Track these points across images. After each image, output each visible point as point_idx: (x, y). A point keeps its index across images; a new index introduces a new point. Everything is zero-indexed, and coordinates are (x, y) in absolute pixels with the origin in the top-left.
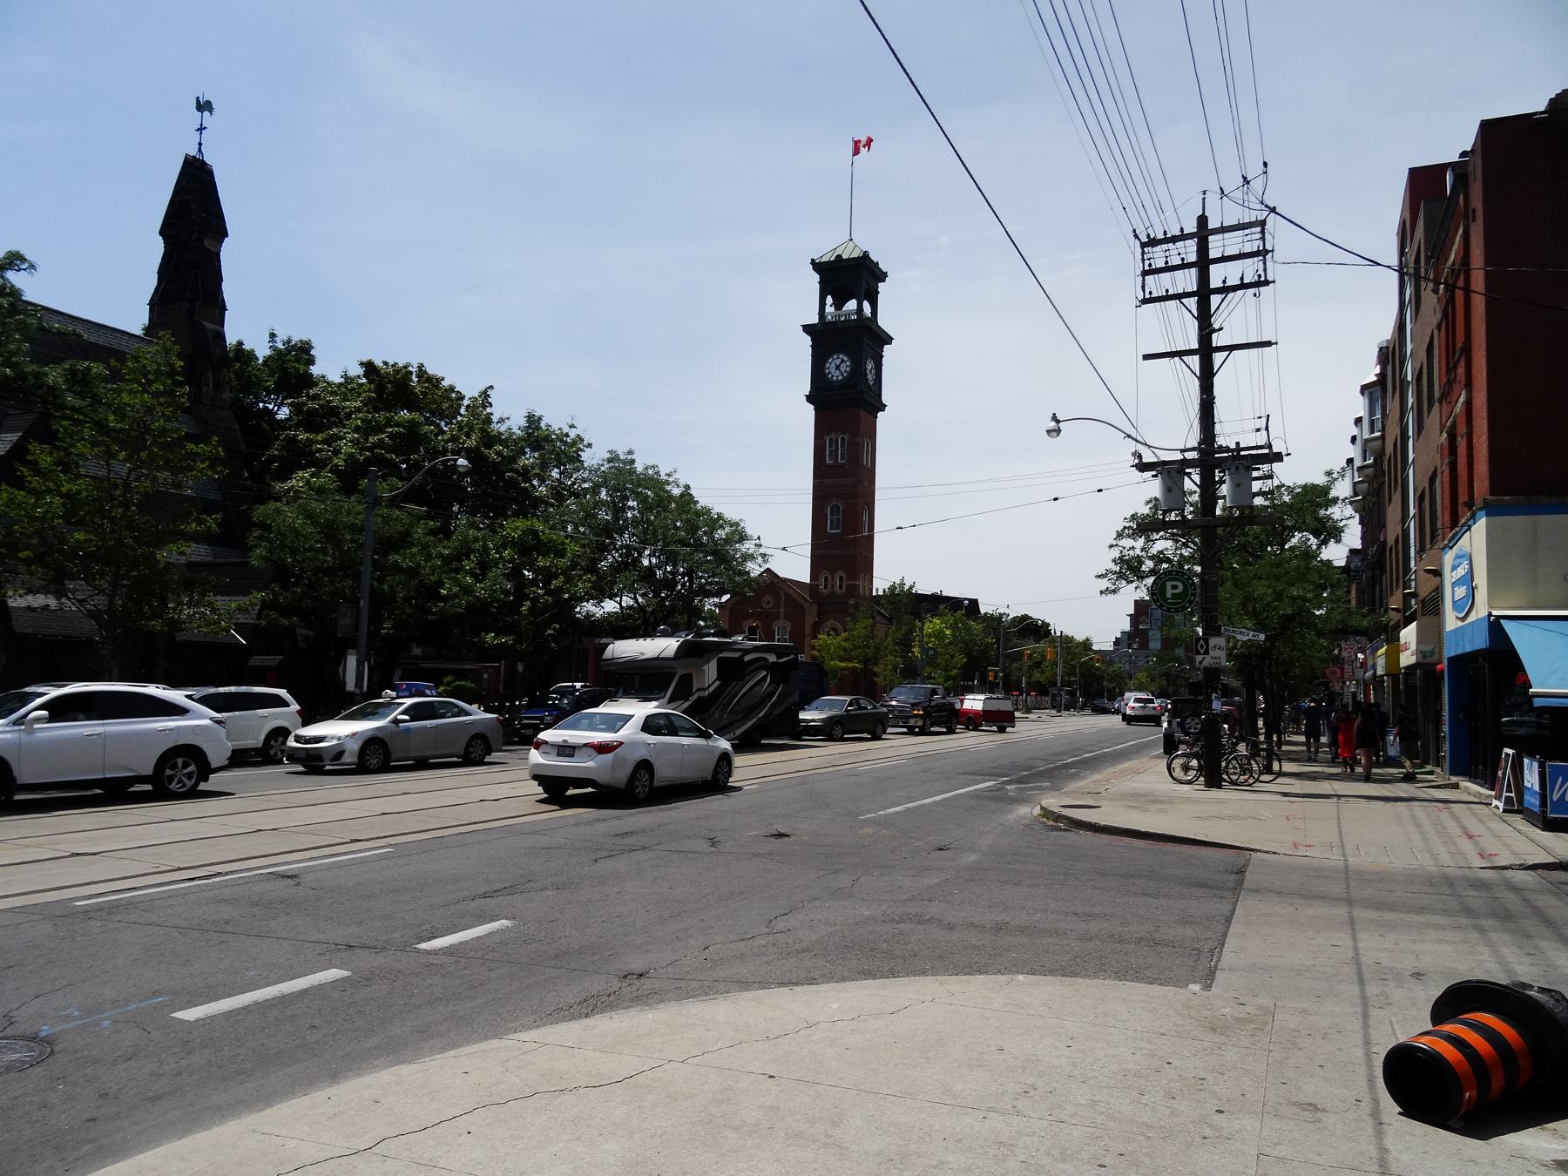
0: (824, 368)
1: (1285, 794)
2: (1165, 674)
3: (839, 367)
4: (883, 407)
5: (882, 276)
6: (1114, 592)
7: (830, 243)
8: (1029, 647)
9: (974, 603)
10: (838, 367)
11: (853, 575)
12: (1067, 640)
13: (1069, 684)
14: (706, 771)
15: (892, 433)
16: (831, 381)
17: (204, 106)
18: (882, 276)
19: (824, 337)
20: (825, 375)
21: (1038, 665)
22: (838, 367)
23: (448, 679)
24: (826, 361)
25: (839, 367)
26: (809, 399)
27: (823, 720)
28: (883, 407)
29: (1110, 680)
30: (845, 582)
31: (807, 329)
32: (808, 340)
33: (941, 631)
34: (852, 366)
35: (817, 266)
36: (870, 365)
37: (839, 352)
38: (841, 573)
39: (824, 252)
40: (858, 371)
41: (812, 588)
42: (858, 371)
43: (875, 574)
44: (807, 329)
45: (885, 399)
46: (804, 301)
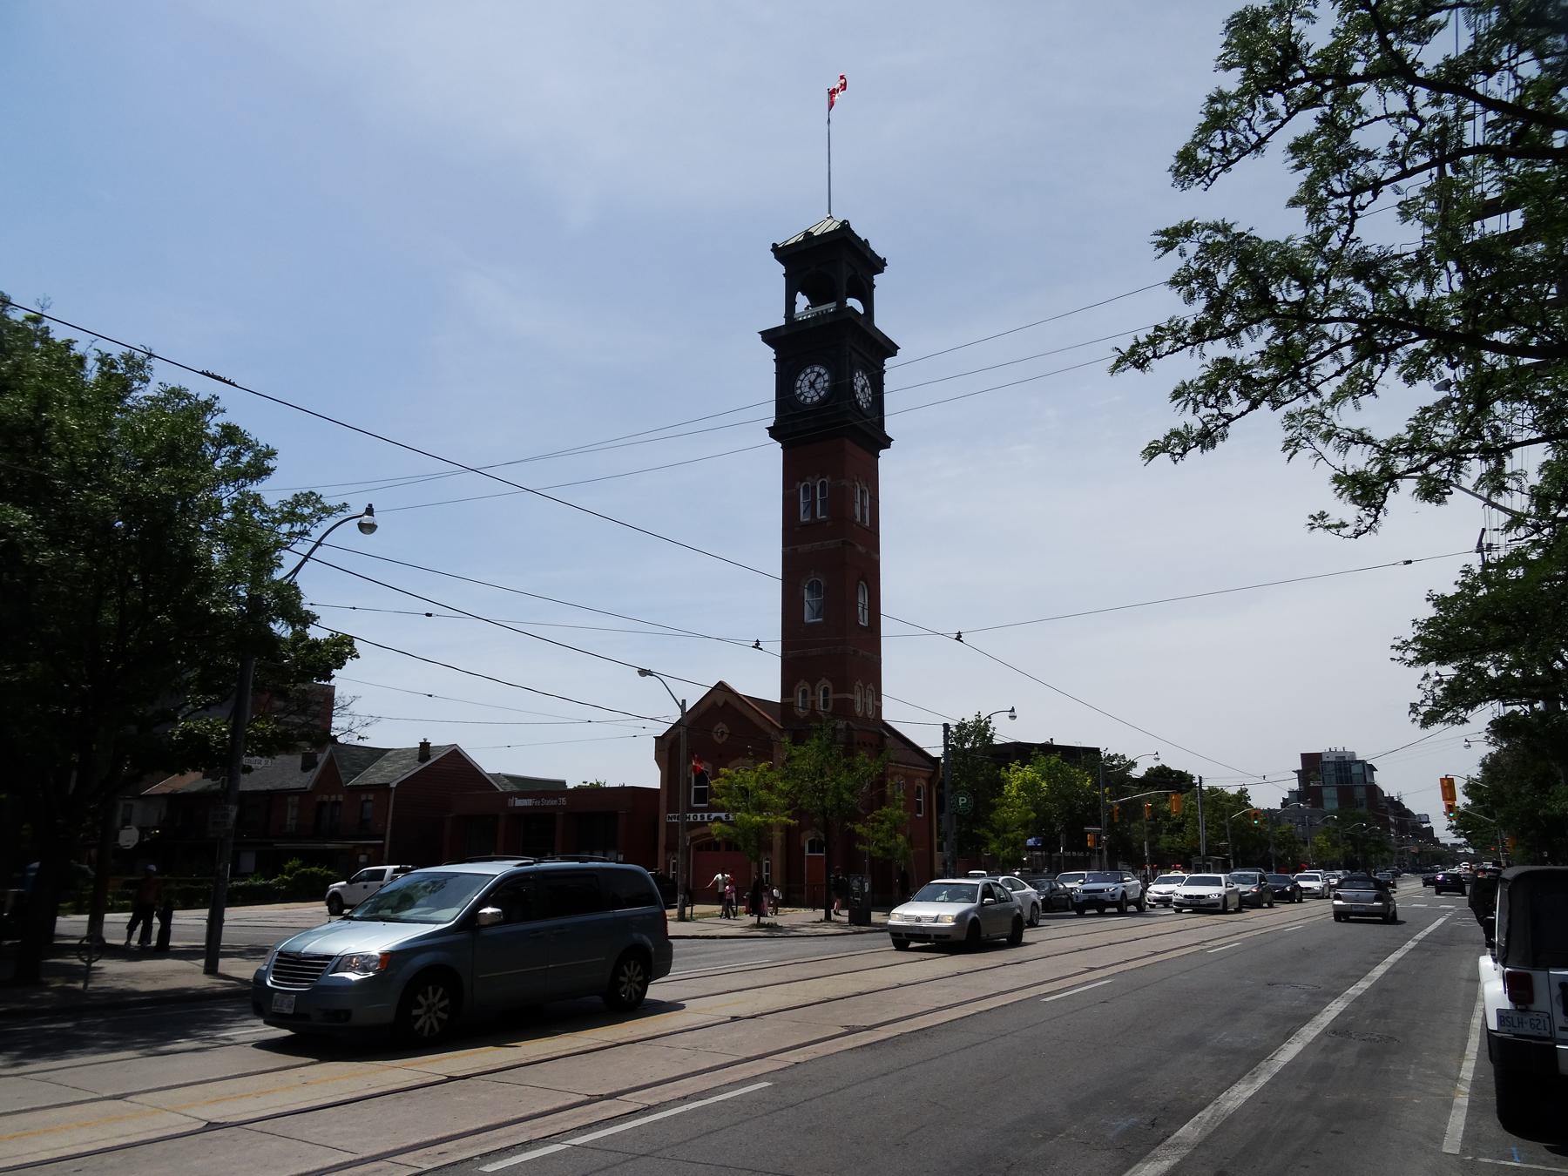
0: (793, 388)
2: (1350, 837)
3: (813, 384)
4: (886, 442)
5: (878, 265)
6: (1207, 439)
8: (1174, 805)
9: (1097, 751)
10: (812, 385)
11: (843, 685)
12: (1216, 796)
13: (1219, 852)
15: (910, 489)
18: (878, 265)
19: (789, 344)
20: (796, 398)
21: (1179, 827)
22: (812, 385)
23: (295, 863)
24: (796, 378)
25: (813, 384)
26: (774, 432)
28: (886, 442)
29: (1279, 846)
30: (831, 696)
31: (769, 336)
32: (770, 353)
33: (1034, 783)
34: (831, 380)
35: (781, 253)
36: (860, 381)
37: (812, 363)
38: (826, 683)
39: (790, 234)
40: (841, 390)
41: (785, 707)
42: (841, 390)
44: (769, 336)
45: (889, 429)
46: (768, 298)
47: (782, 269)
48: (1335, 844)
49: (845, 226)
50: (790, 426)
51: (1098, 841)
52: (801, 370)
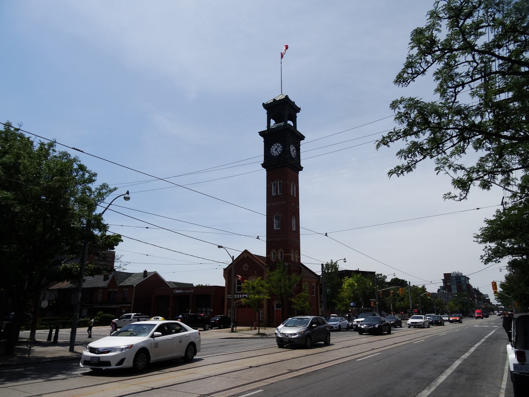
0: (270, 151)
1: (373, 349)
2: (461, 302)
3: (276, 150)
4: (301, 169)
5: (298, 110)
7: (275, 94)
10: (276, 150)
12: (415, 288)
14: (181, 353)
16: (273, 156)
17: (287, 47)
18: (298, 110)
20: (271, 154)
21: (403, 299)
22: (276, 150)
26: (263, 165)
27: (299, 333)
28: (301, 169)
29: (437, 305)
30: (283, 255)
31: (262, 134)
32: (262, 139)
34: (283, 148)
35: (265, 106)
36: (292, 148)
37: (276, 142)
38: (281, 250)
39: (269, 100)
40: (286, 151)
41: (268, 259)
42: (286, 151)
43: (302, 252)
44: (262, 134)
45: (302, 164)
46: (261, 121)
47: (266, 111)
48: (456, 305)
49: (287, 97)
50: (269, 163)
51: (375, 304)
52: (273, 145)
